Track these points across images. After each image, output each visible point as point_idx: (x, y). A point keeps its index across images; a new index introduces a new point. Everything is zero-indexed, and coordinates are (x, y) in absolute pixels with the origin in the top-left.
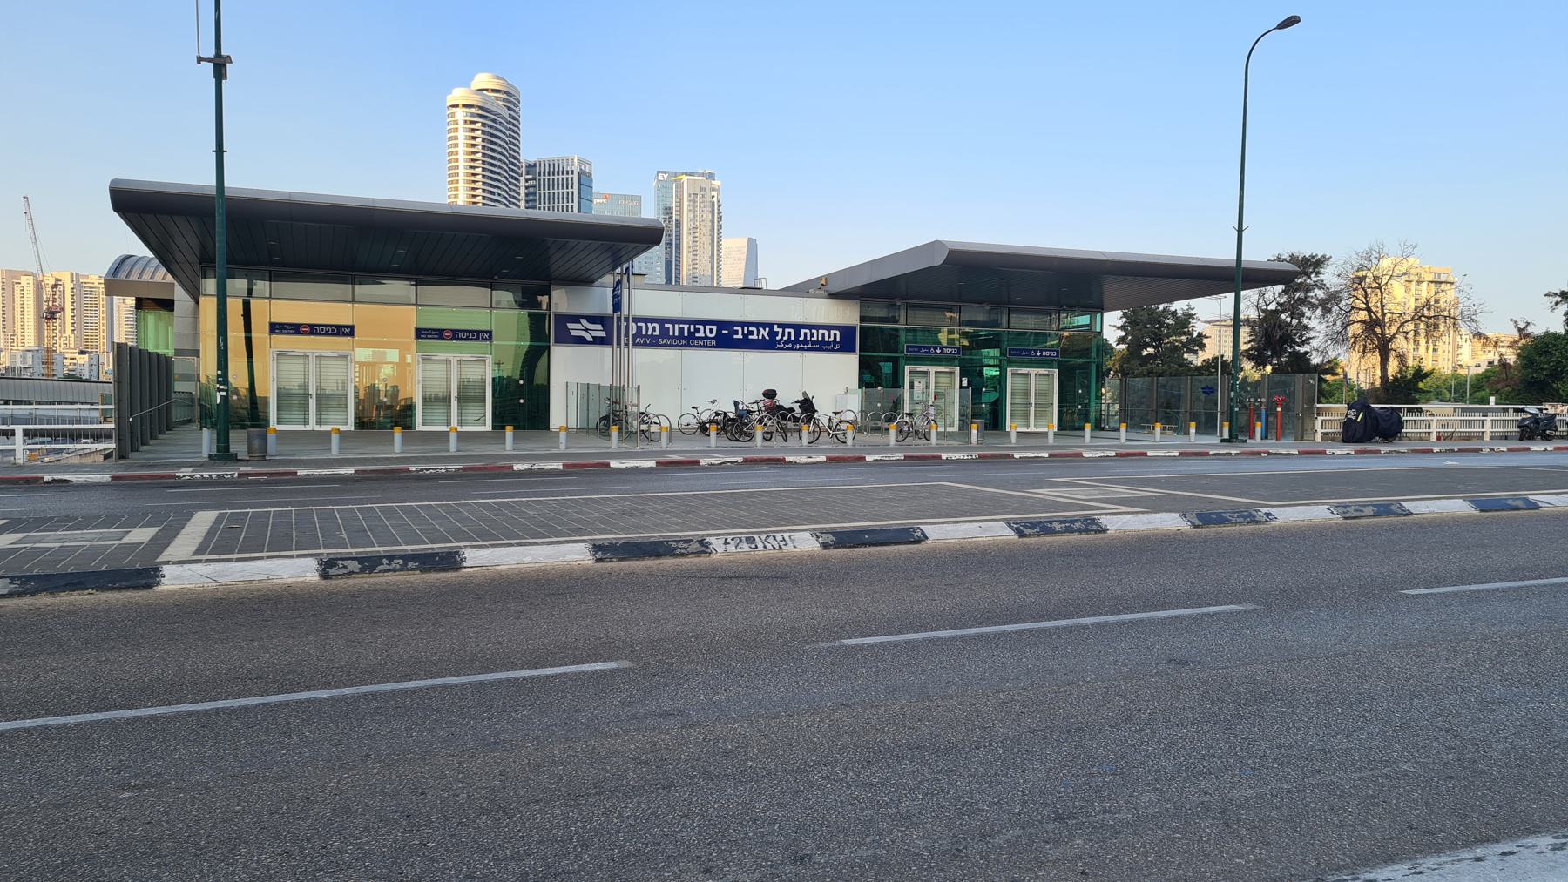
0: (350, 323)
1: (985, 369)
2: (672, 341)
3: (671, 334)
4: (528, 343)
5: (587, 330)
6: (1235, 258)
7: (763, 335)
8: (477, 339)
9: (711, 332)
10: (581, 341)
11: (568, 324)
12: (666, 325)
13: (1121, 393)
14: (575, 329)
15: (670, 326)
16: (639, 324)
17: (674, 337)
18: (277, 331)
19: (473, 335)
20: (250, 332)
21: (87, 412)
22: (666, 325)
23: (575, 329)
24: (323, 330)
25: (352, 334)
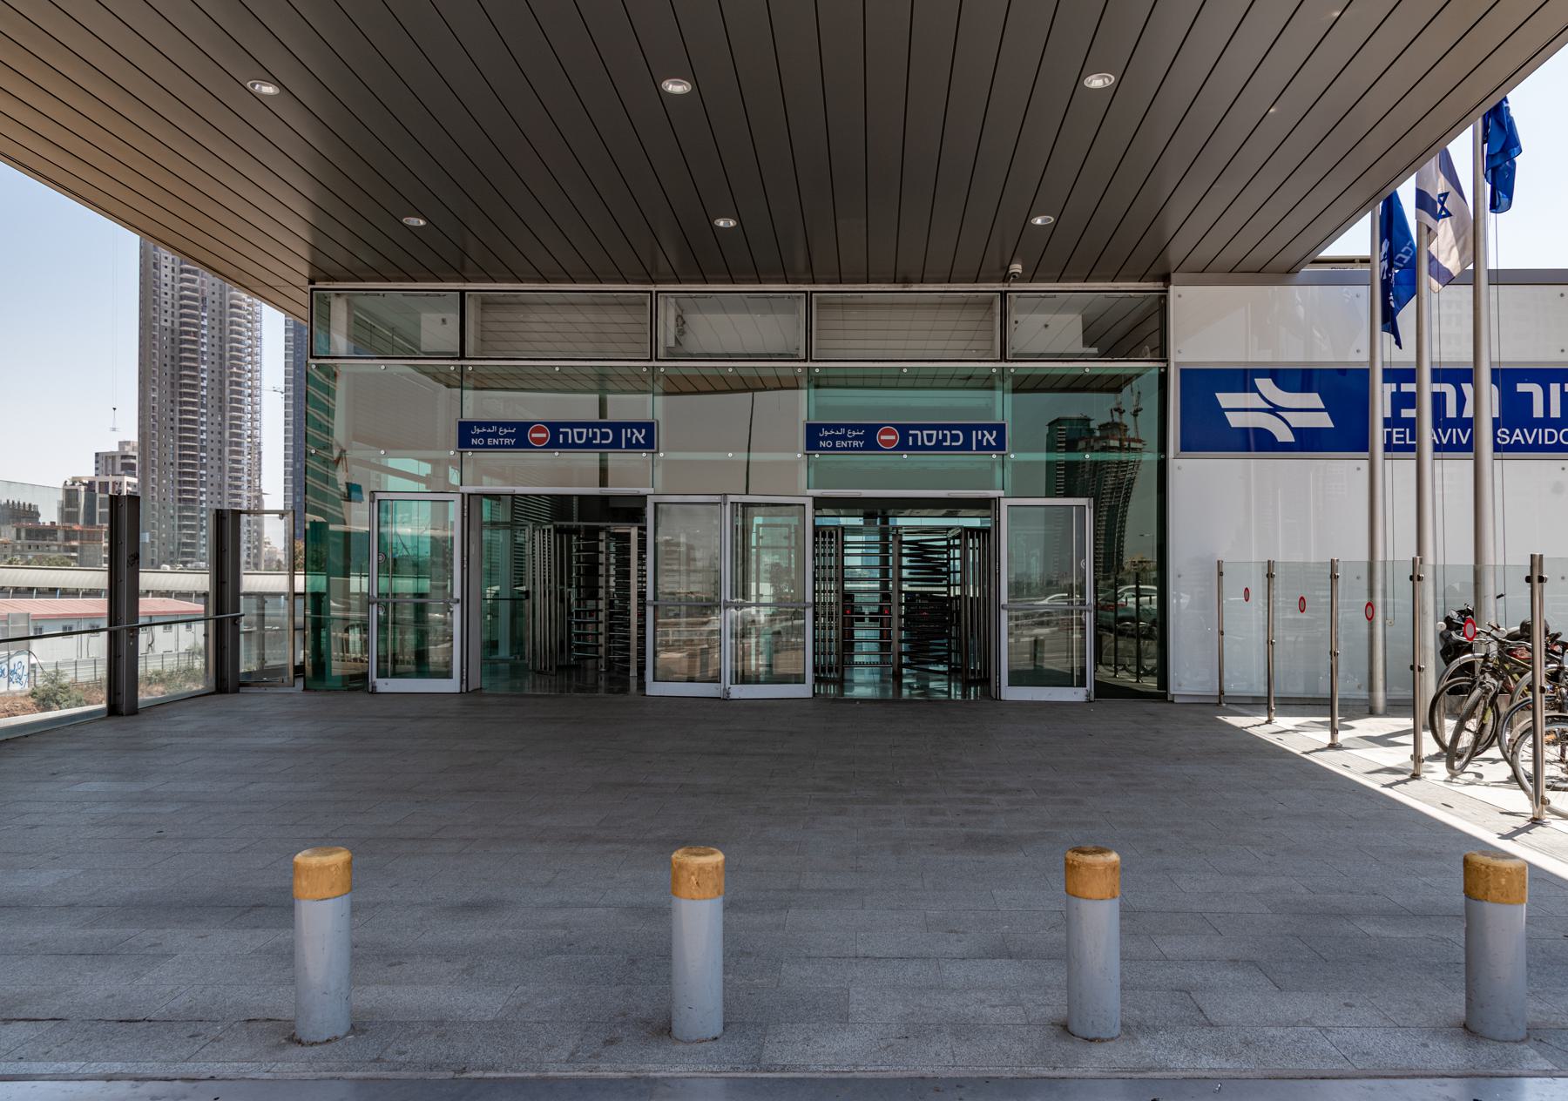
0: (648, 418)
1: (890, 519)
2: (1543, 435)
3: (1538, 412)
4: (1042, 457)
5: (1274, 410)
6: (1472, 360)
7: (991, 435)
8: (966, 446)
9: (580, 437)
10: (1260, 442)
11: (1217, 394)
12: (1522, 388)
13: (1402, 1069)
14: (1241, 411)
15: (1535, 389)
16: (603, 430)
17: (1547, 421)
18: (474, 441)
19: (955, 438)
20: (176, 597)
21: (883, 384)
22: (1522, 388)
23: (1241, 411)
24: (580, 435)
25: (649, 443)
